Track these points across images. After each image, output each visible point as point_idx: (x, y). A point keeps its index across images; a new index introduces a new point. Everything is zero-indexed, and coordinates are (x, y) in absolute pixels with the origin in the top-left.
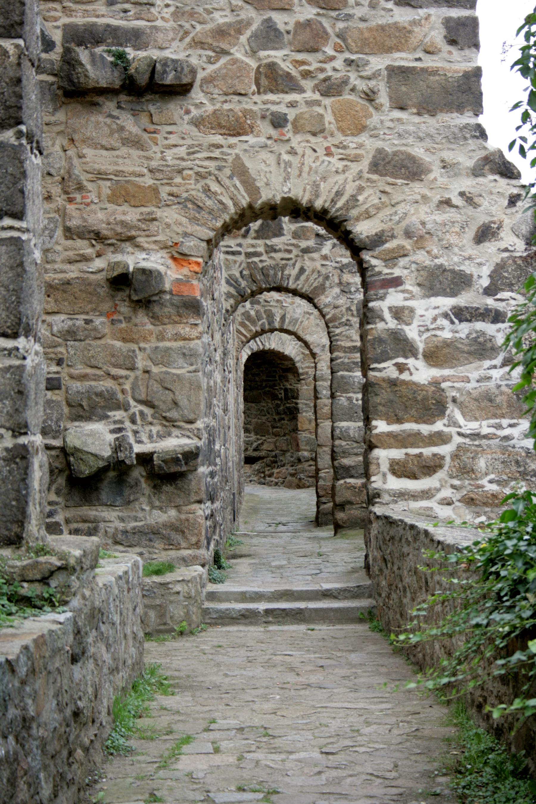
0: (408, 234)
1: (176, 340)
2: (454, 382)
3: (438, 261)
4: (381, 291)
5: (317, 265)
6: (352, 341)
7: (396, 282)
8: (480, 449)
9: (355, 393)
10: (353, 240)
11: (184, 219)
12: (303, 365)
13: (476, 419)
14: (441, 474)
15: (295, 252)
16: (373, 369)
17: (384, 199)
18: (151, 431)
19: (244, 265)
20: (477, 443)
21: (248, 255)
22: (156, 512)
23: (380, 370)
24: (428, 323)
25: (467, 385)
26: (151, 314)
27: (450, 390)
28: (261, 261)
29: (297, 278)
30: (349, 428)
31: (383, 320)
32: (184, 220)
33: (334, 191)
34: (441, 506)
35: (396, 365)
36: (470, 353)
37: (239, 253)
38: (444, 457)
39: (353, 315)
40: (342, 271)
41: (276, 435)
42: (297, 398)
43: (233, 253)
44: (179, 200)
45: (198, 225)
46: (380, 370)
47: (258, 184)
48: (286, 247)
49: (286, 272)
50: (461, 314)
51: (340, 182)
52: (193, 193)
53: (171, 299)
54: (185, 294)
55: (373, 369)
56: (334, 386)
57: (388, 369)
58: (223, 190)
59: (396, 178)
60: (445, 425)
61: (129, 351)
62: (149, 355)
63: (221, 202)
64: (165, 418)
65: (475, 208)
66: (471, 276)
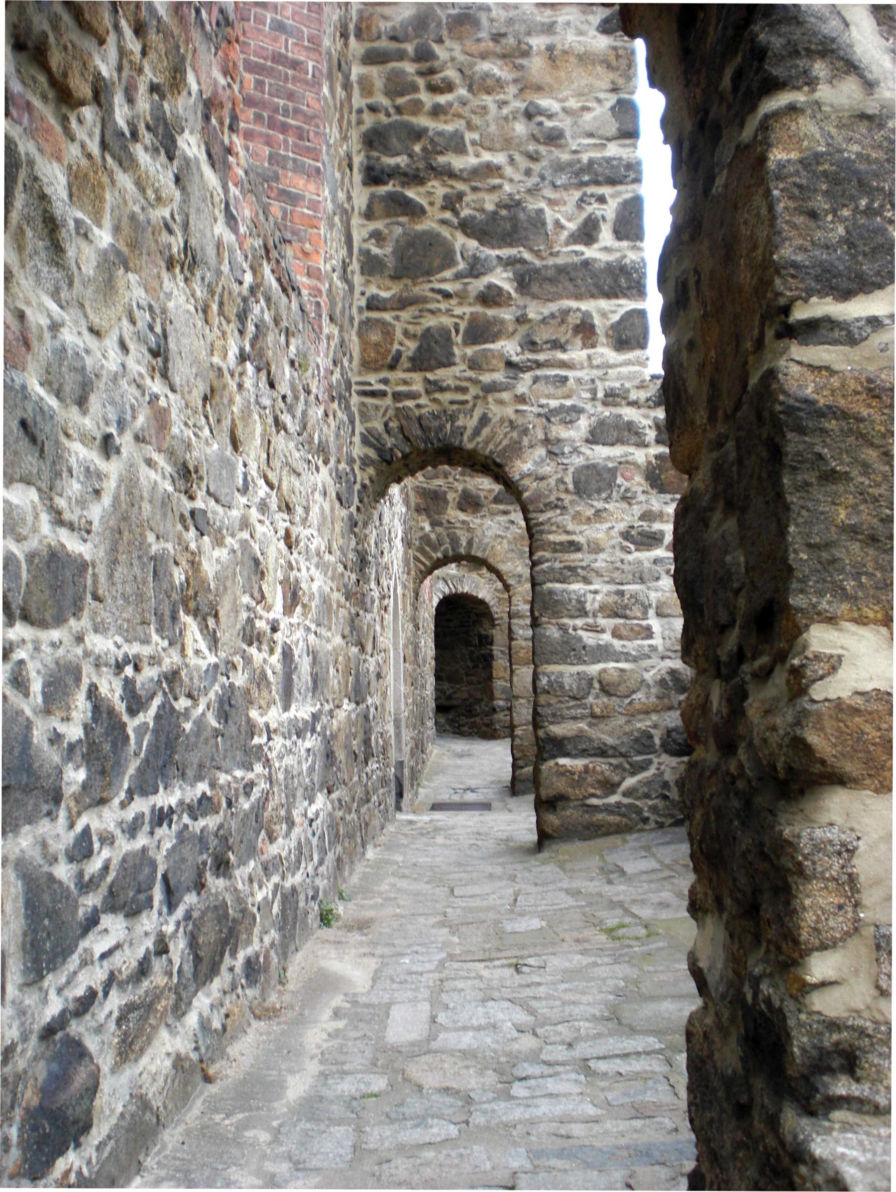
5: (509, 412)
6: (568, 533)
9: (572, 617)
12: (499, 611)
15: (473, 391)
16: (812, 330)
19: (391, 412)
21: (397, 396)
28: (419, 406)
29: (477, 432)
37: (383, 394)
39: (567, 491)
40: (548, 420)
41: (470, 683)
42: (491, 644)
43: (373, 394)
48: (458, 383)
49: (460, 423)
55: (812, 330)
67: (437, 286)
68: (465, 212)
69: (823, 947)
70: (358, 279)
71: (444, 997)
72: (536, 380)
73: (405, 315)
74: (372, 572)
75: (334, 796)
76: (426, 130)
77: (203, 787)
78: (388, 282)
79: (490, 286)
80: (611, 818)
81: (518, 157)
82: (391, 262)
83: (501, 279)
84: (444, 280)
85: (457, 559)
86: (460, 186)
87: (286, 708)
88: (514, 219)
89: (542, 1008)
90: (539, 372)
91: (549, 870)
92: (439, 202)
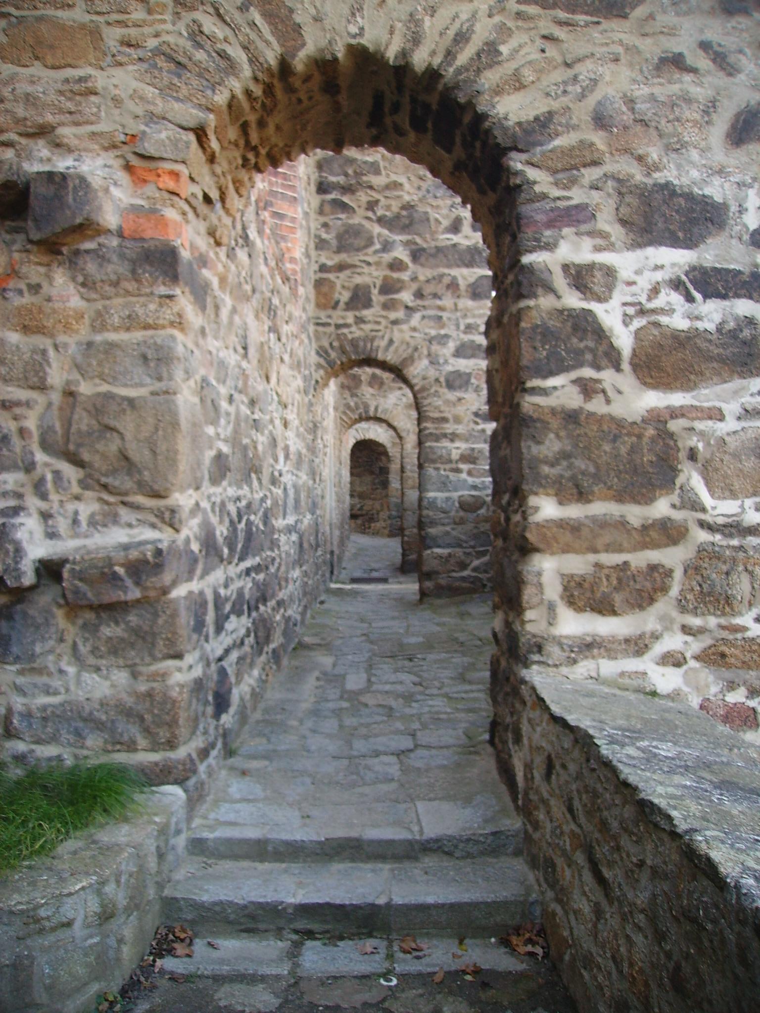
0: (600, 121)
1: (128, 329)
2: (693, 419)
3: (659, 177)
4: (548, 233)
5: (407, 336)
7: (577, 217)
8: (741, 555)
10: (488, 132)
11: (151, 89)
12: (393, 451)
13: (734, 495)
14: (664, 606)
16: (534, 391)
17: (552, 52)
18: (76, 513)
19: (333, 336)
20: (735, 542)
21: (338, 326)
22: (88, 678)
23: (544, 392)
24: (643, 299)
25: (719, 425)
26: (80, 279)
27: (684, 434)
30: (436, 498)
31: (550, 289)
32: (150, 92)
33: (451, 33)
34: (661, 669)
35: (577, 381)
36: (721, 360)
37: (329, 324)
38: (671, 571)
44: (140, 53)
45: (177, 99)
46: (544, 392)
47: (298, 18)
49: (375, 344)
50: (708, 283)
51: (464, 16)
52: (170, 39)
53: (120, 246)
54: (148, 234)
55: (534, 391)
56: (422, 457)
57: (558, 391)
58: (228, 32)
59: (573, 12)
60: (674, 506)
61: (34, 351)
62: (74, 359)
63: (223, 55)
64: (105, 487)
65: (730, 75)
66: (725, 206)
67: (363, 258)
68: (380, 213)
69: (531, 608)
70: (313, 253)
71: (373, 671)
72: (424, 317)
73: (343, 275)
74: (319, 433)
75: (304, 568)
76: (356, 160)
77: (258, 559)
78: (333, 256)
79: (396, 258)
80: (464, 585)
81: (412, 178)
82: (334, 243)
83: (401, 254)
84: (366, 254)
85: (368, 419)
86: (376, 196)
87: (284, 518)
88: (410, 217)
89: (425, 675)
90: (425, 313)
91: (427, 614)
92: (364, 205)
